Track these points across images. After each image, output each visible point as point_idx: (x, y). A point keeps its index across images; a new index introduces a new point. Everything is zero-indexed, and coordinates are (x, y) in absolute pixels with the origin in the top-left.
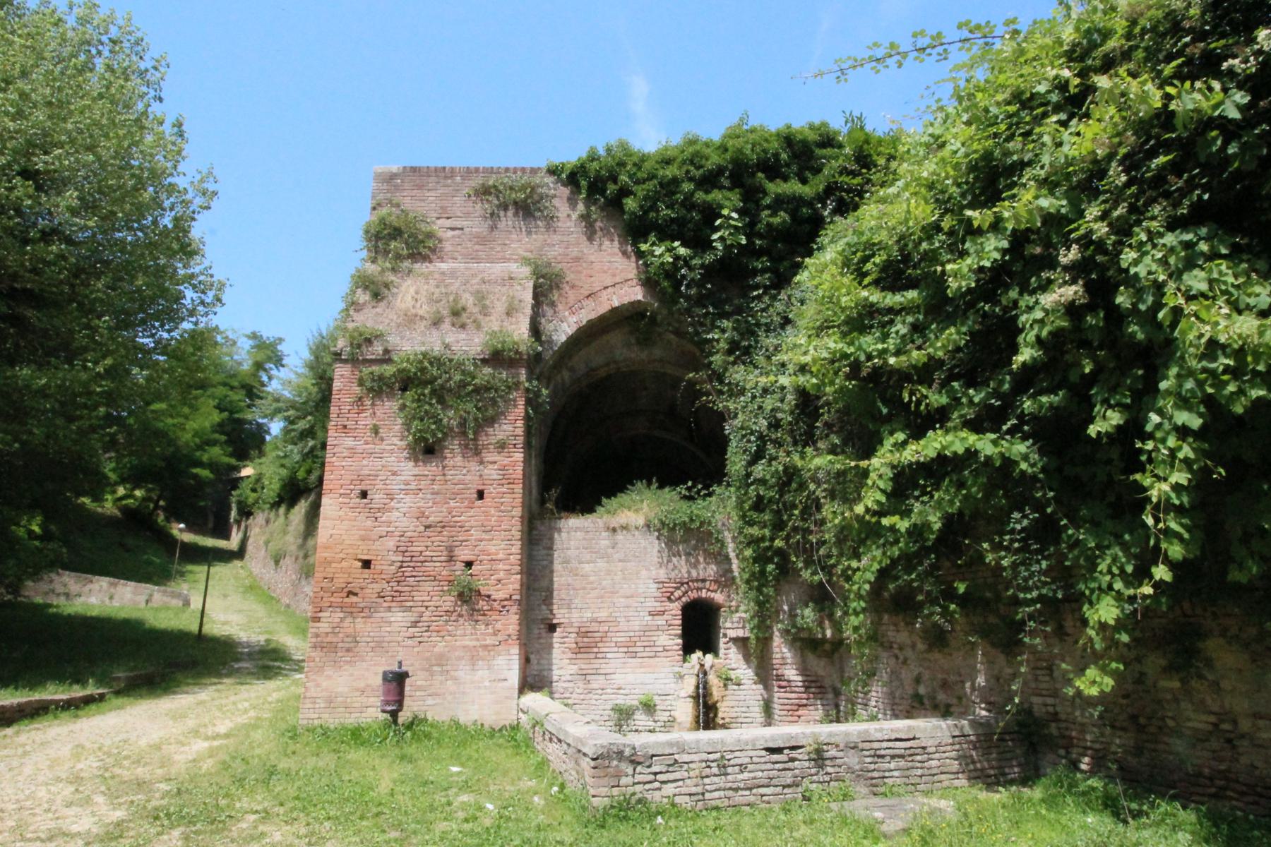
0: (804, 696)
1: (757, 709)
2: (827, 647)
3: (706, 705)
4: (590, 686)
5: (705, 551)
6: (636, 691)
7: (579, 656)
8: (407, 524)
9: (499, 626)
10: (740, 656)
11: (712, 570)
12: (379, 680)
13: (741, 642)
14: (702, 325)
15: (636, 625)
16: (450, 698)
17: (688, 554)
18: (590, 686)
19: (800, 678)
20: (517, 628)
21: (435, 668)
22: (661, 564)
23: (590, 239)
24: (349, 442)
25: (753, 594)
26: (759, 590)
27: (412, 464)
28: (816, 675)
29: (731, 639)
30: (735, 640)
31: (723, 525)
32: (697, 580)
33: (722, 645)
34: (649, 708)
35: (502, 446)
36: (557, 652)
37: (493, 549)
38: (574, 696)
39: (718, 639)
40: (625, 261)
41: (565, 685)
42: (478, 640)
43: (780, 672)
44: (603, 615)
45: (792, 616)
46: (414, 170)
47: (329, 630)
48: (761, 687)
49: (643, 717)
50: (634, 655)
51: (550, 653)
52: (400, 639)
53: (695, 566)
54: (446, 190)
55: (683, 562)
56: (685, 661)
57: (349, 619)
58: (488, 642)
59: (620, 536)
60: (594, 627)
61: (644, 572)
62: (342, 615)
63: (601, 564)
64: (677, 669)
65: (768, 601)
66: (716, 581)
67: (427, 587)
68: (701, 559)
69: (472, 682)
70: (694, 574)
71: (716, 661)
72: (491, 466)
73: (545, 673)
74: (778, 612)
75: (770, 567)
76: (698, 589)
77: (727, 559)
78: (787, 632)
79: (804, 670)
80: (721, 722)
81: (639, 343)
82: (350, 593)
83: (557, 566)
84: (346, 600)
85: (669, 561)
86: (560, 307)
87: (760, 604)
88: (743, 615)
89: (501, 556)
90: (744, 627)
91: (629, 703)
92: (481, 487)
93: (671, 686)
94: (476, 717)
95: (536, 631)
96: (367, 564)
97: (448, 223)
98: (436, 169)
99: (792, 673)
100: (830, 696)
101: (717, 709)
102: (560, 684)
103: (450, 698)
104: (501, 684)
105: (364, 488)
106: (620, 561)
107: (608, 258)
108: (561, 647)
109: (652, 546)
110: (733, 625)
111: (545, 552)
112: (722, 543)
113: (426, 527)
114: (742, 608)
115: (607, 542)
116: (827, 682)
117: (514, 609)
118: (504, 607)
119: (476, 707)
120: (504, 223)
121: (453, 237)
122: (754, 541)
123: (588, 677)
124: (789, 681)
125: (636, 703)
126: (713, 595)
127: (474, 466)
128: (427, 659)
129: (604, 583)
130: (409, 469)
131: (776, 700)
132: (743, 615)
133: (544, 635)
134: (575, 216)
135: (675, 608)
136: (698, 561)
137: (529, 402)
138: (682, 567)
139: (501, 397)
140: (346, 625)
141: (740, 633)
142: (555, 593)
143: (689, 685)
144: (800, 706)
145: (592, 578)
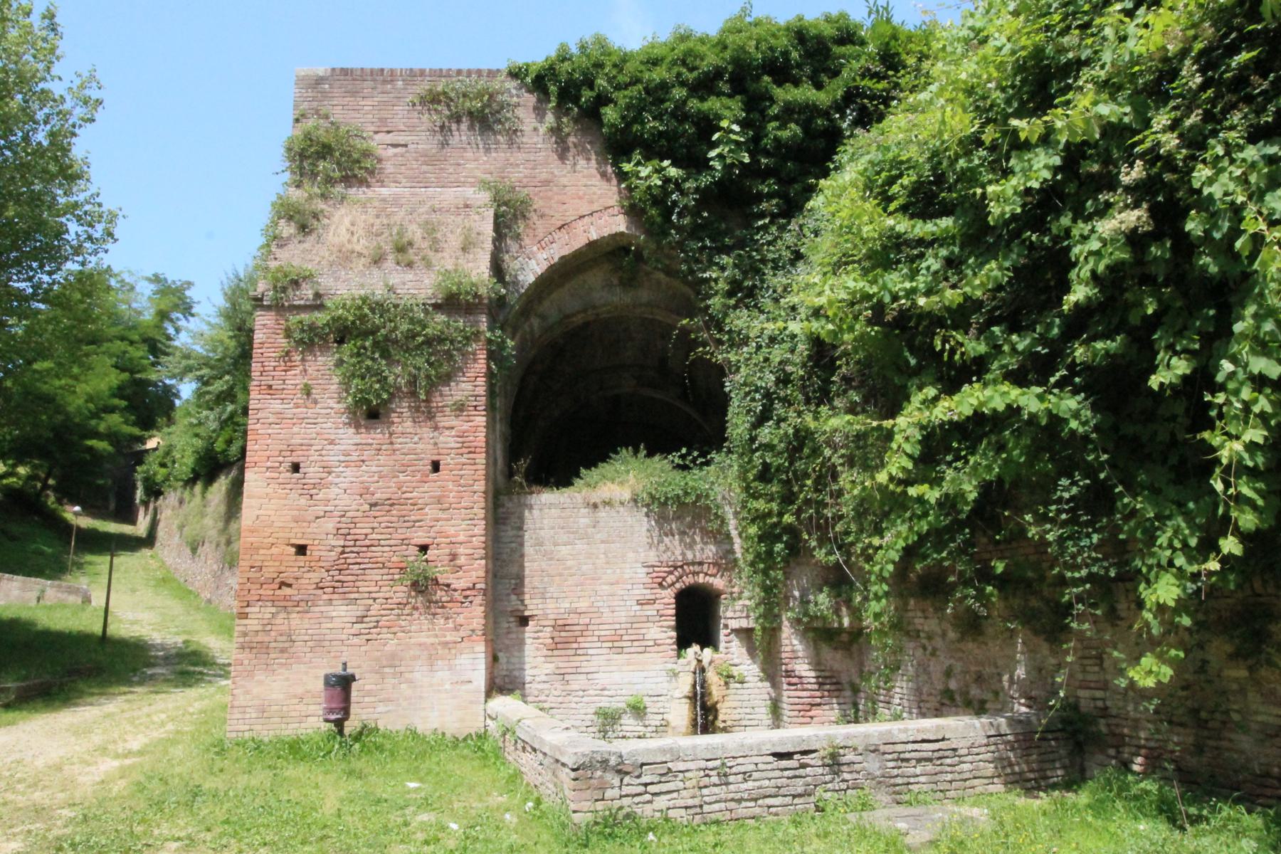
0: (818, 694)
1: (764, 710)
2: (845, 637)
3: (704, 707)
4: (568, 687)
5: (702, 529)
6: (624, 692)
7: (556, 653)
9: (460, 619)
10: (744, 650)
11: (710, 551)
12: (320, 684)
13: (745, 634)
15: (622, 616)
16: (404, 704)
17: (683, 533)
18: (568, 687)
19: (813, 674)
20: (483, 621)
21: (387, 670)
22: (651, 545)
23: (562, 157)
24: (276, 405)
25: (758, 578)
26: (765, 573)
27: (352, 430)
28: (831, 670)
30: (737, 632)
31: (724, 498)
32: (693, 563)
33: (722, 638)
34: (638, 710)
35: (460, 408)
37: (452, 531)
38: (551, 698)
39: (718, 631)
40: (604, 184)
41: (541, 686)
42: (436, 636)
43: (790, 667)
44: (583, 605)
45: (804, 602)
46: (345, 72)
48: (767, 684)
49: (632, 721)
51: (521, 650)
52: (344, 637)
53: (691, 546)
54: (385, 98)
55: (677, 543)
56: (679, 656)
57: (283, 615)
58: (448, 638)
59: (603, 513)
60: (573, 619)
61: (631, 555)
63: (580, 546)
64: (670, 666)
65: (776, 586)
66: (715, 564)
67: (375, 575)
68: (698, 539)
70: (690, 556)
71: (716, 656)
72: (447, 433)
73: (516, 673)
74: (787, 598)
75: (779, 547)
76: (695, 573)
77: (728, 536)
78: (799, 621)
79: (817, 665)
83: (528, 549)
86: (527, 241)
87: (767, 590)
88: (747, 602)
89: (461, 538)
90: (748, 617)
91: (615, 705)
92: (435, 458)
96: (301, 550)
97: (389, 138)
99: (803, 669)
100: (848, 693)
101: (716, 711)
102: (534, 686)
104: (465, 687)
105: (296, 460)
106: (603, 542)
109: (640, 525)
110: (736, 613)
111: (511, 533)
113: (373, 505)
114: (746, 594)
116: (844, 679)
117: (479, 599)
120: (457, 138)
121: (395, 155)
122: (759, 517)
123: (567, 677)
124: (801, 677)
125: (623, 705)
126: (711, 580)
127: (426, 432)
129: (584, 567)
130: (349, 437)
131: (785, 699)
132: (747, 602)
133: (515, 629)
134: (543, 129)
135: (668, 596)
136: (694, 542)
137: (491, 356)
138: (675, 549)
141: (744, 624)
142: (527, 581)
143: (685, 684)
144: (813, 705)
145: (569, 563)
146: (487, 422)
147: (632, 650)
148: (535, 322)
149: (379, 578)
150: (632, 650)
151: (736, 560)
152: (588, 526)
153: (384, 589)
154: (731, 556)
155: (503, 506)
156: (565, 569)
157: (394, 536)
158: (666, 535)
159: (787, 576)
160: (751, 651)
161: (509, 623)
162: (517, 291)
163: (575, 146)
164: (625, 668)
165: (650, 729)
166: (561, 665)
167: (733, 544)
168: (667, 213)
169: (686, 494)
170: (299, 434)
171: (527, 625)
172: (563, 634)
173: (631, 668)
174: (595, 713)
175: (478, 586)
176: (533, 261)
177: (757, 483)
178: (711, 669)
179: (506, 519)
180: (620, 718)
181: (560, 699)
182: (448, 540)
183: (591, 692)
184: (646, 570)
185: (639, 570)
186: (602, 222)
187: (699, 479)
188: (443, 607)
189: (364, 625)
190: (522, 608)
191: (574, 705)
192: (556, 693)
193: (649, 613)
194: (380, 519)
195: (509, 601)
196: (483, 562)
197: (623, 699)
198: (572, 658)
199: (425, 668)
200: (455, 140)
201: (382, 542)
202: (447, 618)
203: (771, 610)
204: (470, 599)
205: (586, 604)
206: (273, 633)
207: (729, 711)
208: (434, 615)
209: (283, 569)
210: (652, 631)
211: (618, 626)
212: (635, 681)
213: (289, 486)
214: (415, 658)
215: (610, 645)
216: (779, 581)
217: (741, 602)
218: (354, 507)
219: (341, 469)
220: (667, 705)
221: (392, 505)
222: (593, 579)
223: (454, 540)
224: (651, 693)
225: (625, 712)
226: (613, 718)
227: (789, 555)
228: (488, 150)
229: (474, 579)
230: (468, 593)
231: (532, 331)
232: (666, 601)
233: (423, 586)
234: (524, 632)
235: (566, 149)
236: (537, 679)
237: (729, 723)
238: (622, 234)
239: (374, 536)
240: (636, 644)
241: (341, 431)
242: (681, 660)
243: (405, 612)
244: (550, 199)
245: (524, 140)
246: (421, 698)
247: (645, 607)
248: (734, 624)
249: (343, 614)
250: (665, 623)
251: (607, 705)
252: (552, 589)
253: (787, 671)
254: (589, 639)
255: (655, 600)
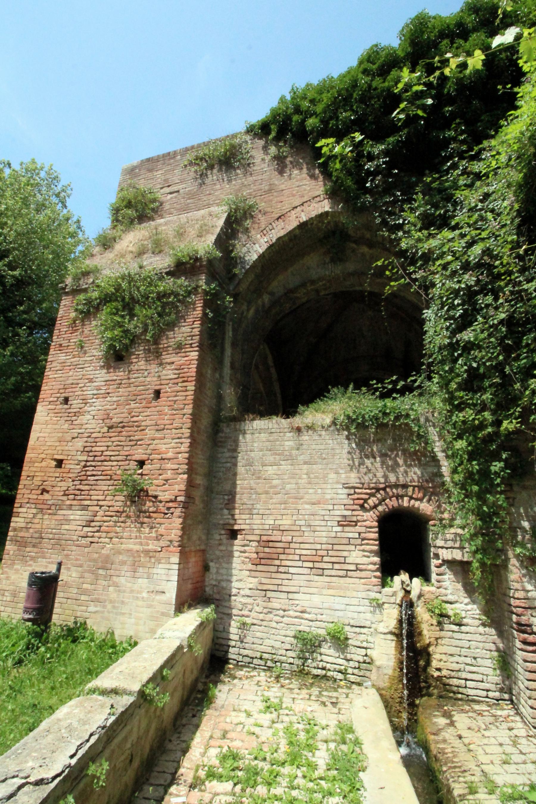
3: (411, 647)
4: (270, 605)
5: (404, 451)
7: (260, 568)
8: (93, 426)
9: (162, 530)
10: (459, 586)
11: (415, 474)
12: (24, 584)
13: (460, 568)
14: (391, 214)
15: (323, 536)
16: (109, 606)
17: (384, 455)
18: (270, 605)
20: (180, 533)
21: (101, 572)
23: (281, 172)
24: (62, 357)
25: (472, 503)
26: (481, 496)
27: (105, 371)
29: (445, 562)
30: (451, 564)
31: (427, 420)
32: (396, 486)
33: (434, 569)
34: (340, 642)
35: (180, 347)
36: (236, 562)
37: (163, 448)
38: (253, 614)
39: (429, 558)
40: (313, 182)
42: (141, 544)
43: (524, 619)
44: (286, 522)
46: (148, 160)
47: (23, 525)
48: (493, 631)
49: (332, 652)
50: (321, 573)
51: (230, 562)
52: (75, 538)
53: (394, 468)
54: (169, 167)
55: (378, 465)
56: (384, 585)
57: (40, 516)
58: (151, 547)
59: (305, 437)
60: (276, 536)
61: (332, 476)
62: (34, 511)
63: (285, 467)
64: (373, 595)
65: (496, 514)
66: (420, 488)
67: (103, 486)
68: (401, 461)
69: (132, 591)
70: (392, 478)
71: (427, 588)
72: (168, 367)
73: (224, 584)
75: (496, 466)
76: (399, 497)
77: (435, 460)
80: (436, 674)
81: (333, 260)
82: (44, 491)
83: (241, 469)
84: (40, 497)
85: (361, 464)
86: (253, 232)
88: (460, 531)
89: (170, 455)
90: (462, 548)
92: (157, 388)
93: (366, 616)
94: (132, 633)
95: (217, 537)
96: (60, 463)
97: (167, 190)
98: (164, 156)
101: (429, 655)
102: (239, 599)
103: (109, 606)
104: (159, 597)
105: (66, 395)
106: (305, 463)
107: (298, 183)
108: (241, 555)
110: (448, 543)
111: (227, 454)
112: (423, 438)
113: (110, 428)
114: (458, 522)
115: (291, 443)
117: (178, 512)
118: (168, 509)
119: (133, 620)
120: (210, 179)
121: (172, 198)
122: (466, 430)
123: (269, 594)
125: (323, 632)
126: (417, 504)
127: (154, 368)
128: (95, 560)
129: (288, 487)
130: (102, 375)
132: (460, 531)
133: (225, 541)
134: (268, 158)
135: (370, 519)
136: (397, 464)
137: (206, 305)
138: (377, 471)
139: (179, 301)
140: (36, 521)
141: (457, 555)
142: (238, 496)
143: (390, 617)
145: (275, 482)
146: (199, 356)
147: (333, 573)
148: (266, 298)
149: (106, 488)
150: (333, 573)
151: (443, 484)
152: (292, 449)
153: (108, 498)
154: (438, 480)
155: (222, 431)
156: (271, 487)
157: (122, 453)
158: (367, 457)
159: (511, 501)
160: (469, 589)
161: (219, 535)
162: (244, 268)
163: (291, 162)
164: (325, 591)
165: (352, 664)
166: (264, 581)
167: (439, 467)
168: (360, 183)
169: (385, 414)
170: (73, 376)
171: (236, 538)
172: (267, 550)
173: (331, 592)
174: (295, 637)
175: (179, 499)
176: (257, 245)
177: (462, 394)
178: (420, 603)
179: (225, 442)
180: (320, 646)
181: (261, 616)
182: (159, 457)
183: (291, 613)
184: (346, 491)
185: (340, 491)
186: (311, 208)
187: (404, 403)
188: (149, 517)
189: (90, 529)
190: (232, 522)
191: (274, 625)
192: (258, 609)
193: (351, 535)
194: (113, 439)
195: (222, 515)
196: (186, 476)
197: (323, 625)
198: (274, 575)
199: (128, 574)
200: (208, 181)
201: (113, 458)
202: (152, 528)
203: (492, 542)
204: (172, 510)
205: (289, 522)
206: (31, 531)
207: (444, 657)
208: (142, 523)
209: (46, 478)
210: (354, 554)
211: (318, 547)
212: (337, 607)
213: (60, 415)
214: (123, 563)
215: (310, 565)
216: (500, 507)
217: (452, 530)
218: (98, 430)
219: (94, 400)
220: (370, 639)
221: (123, 427)
222: (296, 498)
223: (164, 456)
224: (352, 622)
225: (325, 640)
226: (313, 645)
227: (511, 476)
228: (230, 181)
229: (176, 492)
230: (171, 504)
231: (263, 305)
232: (368, 523)
233: (138, 495)
234: (233, 545)
235: (285, 166)
236: (242, 592)
237: (444, 673)
238: (327, 213)
239: (108, 453)
240: (336, 566)
241: (97, 372)
242: (387, 590)
243: (121, 519)
244: (271, 201)
245: (255, 168)
246: (123, 602)
247: (347, 529)
248: (446, 555)
249: (78, 517)
250: (368, 548)
251: (307, 629)
252: (258, 506)
253: (519, 624)
254: (291, 557)
255: (356, 522)
